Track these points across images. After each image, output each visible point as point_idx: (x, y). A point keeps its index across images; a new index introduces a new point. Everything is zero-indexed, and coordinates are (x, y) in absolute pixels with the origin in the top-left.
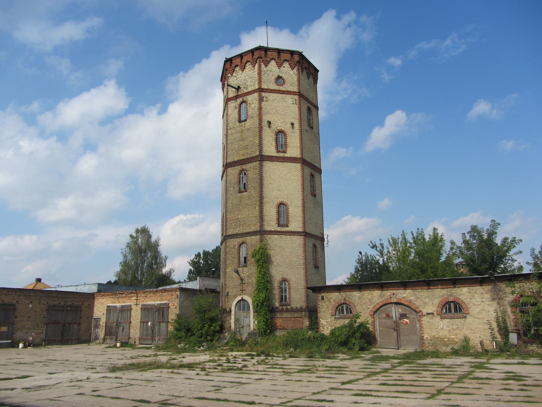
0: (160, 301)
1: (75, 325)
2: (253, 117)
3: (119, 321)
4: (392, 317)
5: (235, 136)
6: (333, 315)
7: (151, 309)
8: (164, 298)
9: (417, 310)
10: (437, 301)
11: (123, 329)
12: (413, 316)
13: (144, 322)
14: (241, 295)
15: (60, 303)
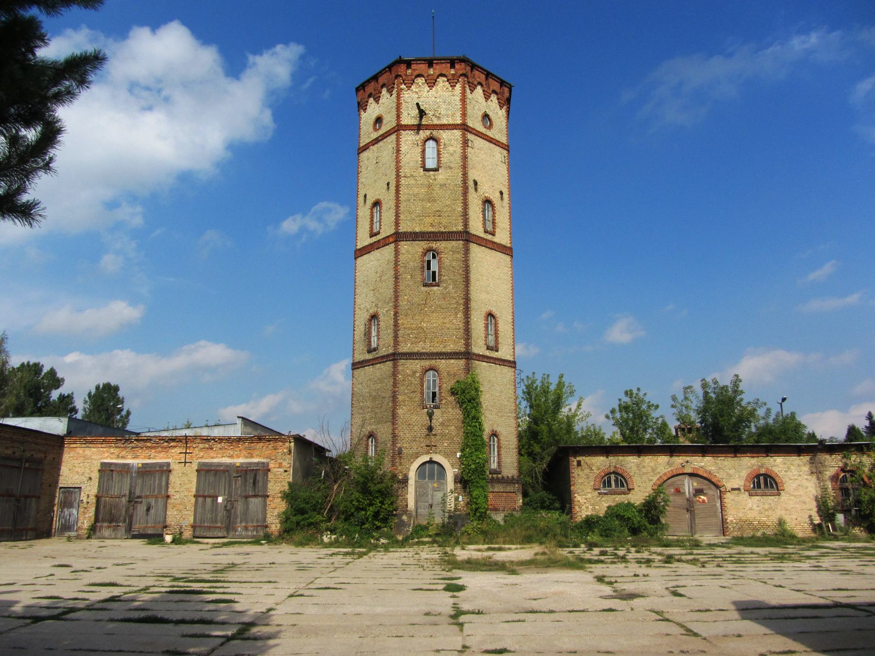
0: (247, 457)
1: (34, 499)
2: (451, 168)
3: (138, 493)
4: (684, 493)
5: (416, 190)
6: (595, 489)
7: (224, 471)
8: (255, 453)
9: (719, 484)
10: (744, 473)
11: (148, 510)
12: (712, 492)
13: (205, 497)
14: (428, 453)
15: (14, 453)
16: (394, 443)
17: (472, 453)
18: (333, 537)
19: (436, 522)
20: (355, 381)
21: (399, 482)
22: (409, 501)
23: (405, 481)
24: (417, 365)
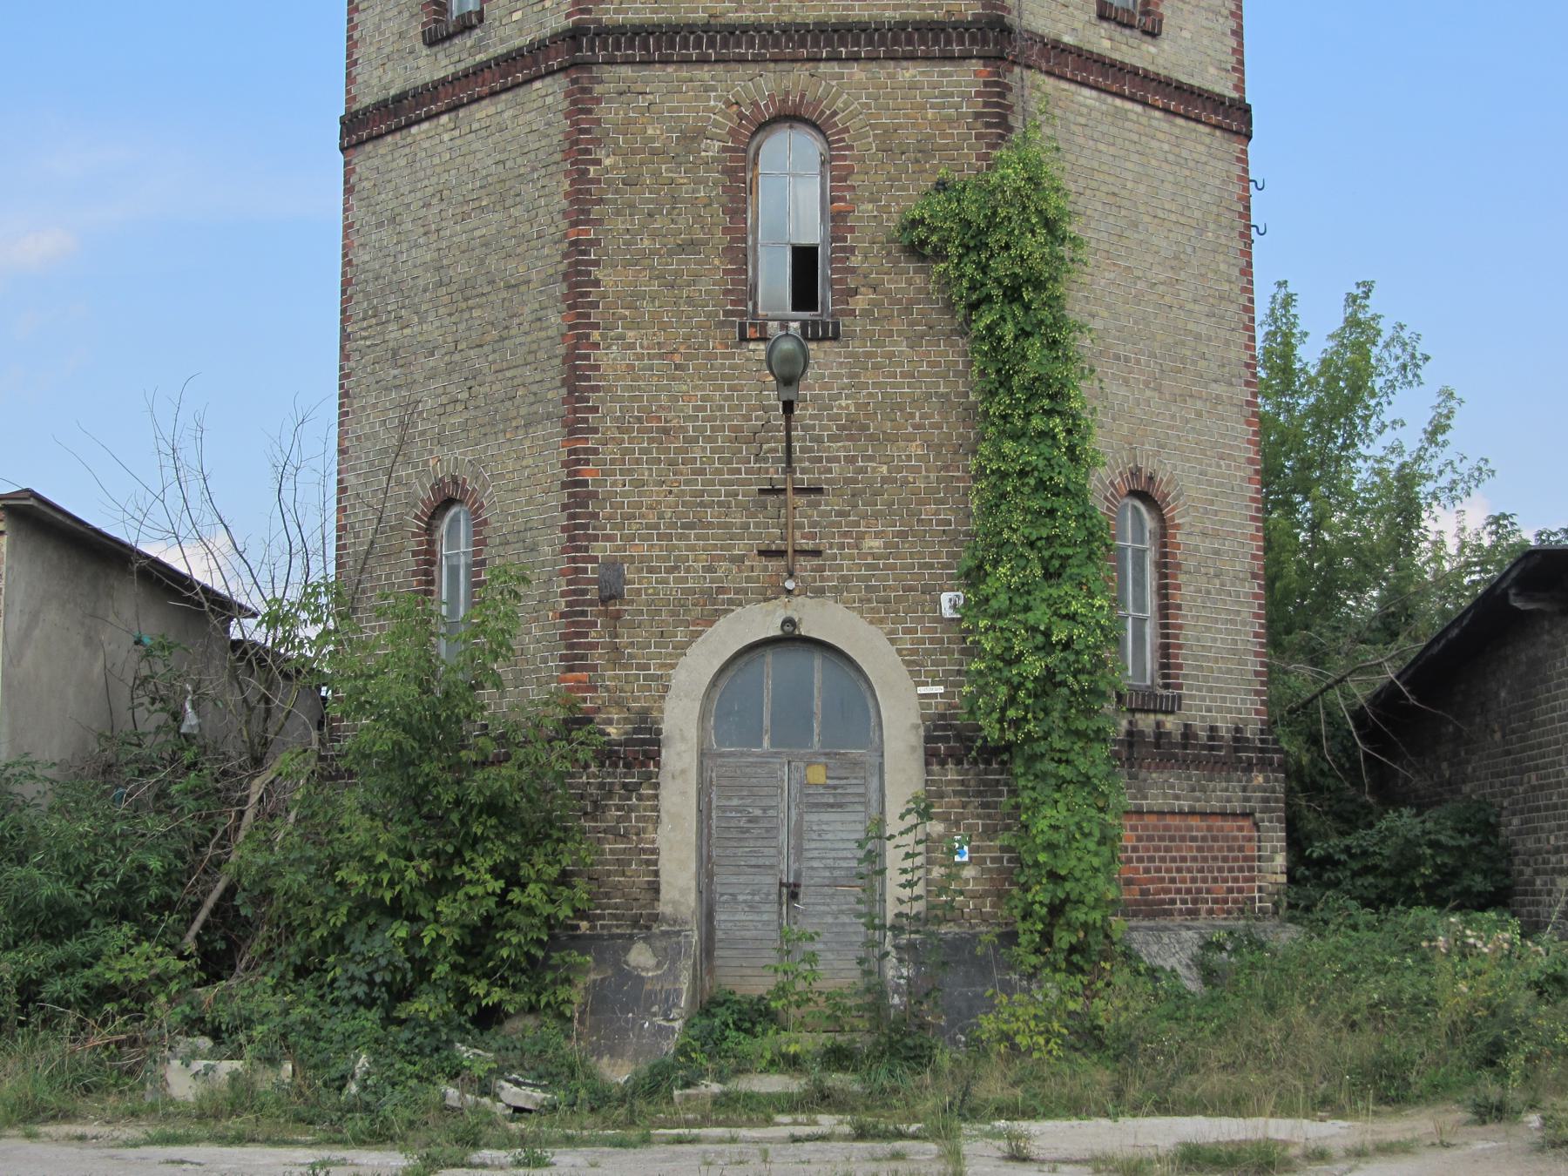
14: (773, 592)
16: (577, 537)
17: (1025, 589)
18: (226, 1067)
19: (826, 984)
20: (358, 212)
21: (608, 755)
22: (667, 865)
23: (642, 750)
24: (707, 95)
